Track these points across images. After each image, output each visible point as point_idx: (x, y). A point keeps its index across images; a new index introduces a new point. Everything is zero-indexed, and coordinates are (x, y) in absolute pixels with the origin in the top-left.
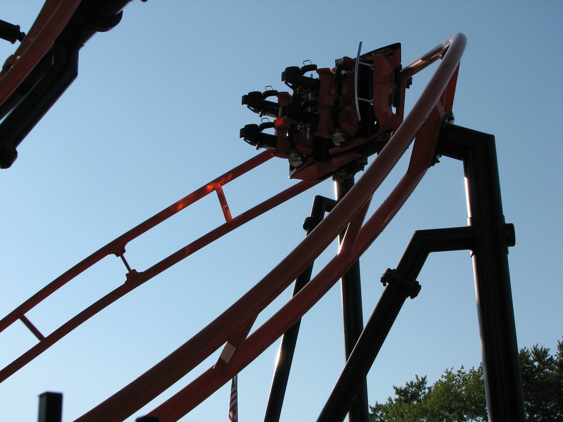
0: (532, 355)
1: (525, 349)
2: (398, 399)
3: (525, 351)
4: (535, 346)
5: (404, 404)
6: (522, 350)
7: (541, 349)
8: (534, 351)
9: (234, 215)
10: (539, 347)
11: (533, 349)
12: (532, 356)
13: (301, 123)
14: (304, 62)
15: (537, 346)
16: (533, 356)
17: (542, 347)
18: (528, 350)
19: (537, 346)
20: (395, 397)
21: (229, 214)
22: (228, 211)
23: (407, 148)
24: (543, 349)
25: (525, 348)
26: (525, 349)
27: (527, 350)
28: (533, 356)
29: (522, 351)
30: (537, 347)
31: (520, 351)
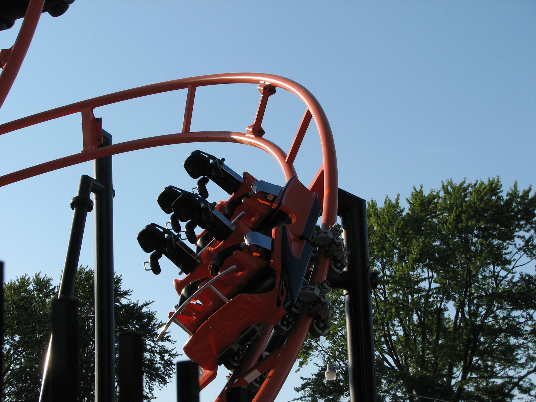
0: (33, 283)
1: (25, 276)
2: (509, 343)
3: (27, 278)
4: (37, 275)
5: (526, 353)
6: (23, 277)
7: (44, 279)
8: (35, 279)
9: (193, 129)
10: (42, 276)
11: (35, 277)
12: (32, 285)
13: (394, 354)
14: (166, 223)
15: (39, 274)
16: (34, 285)
17: (45, 276)
18: (29, 277)
19: (39, 274)
20: (380, 205)
21: (454, 329)
22: (188, 107)
23: (389, 365)
24: (45, 279)
25: (26, 275)
26: (25, 276)
27: (28, 278)
28: (34, 285)
29: (23, 279)
30: (40, 275)
31: (21, 278)
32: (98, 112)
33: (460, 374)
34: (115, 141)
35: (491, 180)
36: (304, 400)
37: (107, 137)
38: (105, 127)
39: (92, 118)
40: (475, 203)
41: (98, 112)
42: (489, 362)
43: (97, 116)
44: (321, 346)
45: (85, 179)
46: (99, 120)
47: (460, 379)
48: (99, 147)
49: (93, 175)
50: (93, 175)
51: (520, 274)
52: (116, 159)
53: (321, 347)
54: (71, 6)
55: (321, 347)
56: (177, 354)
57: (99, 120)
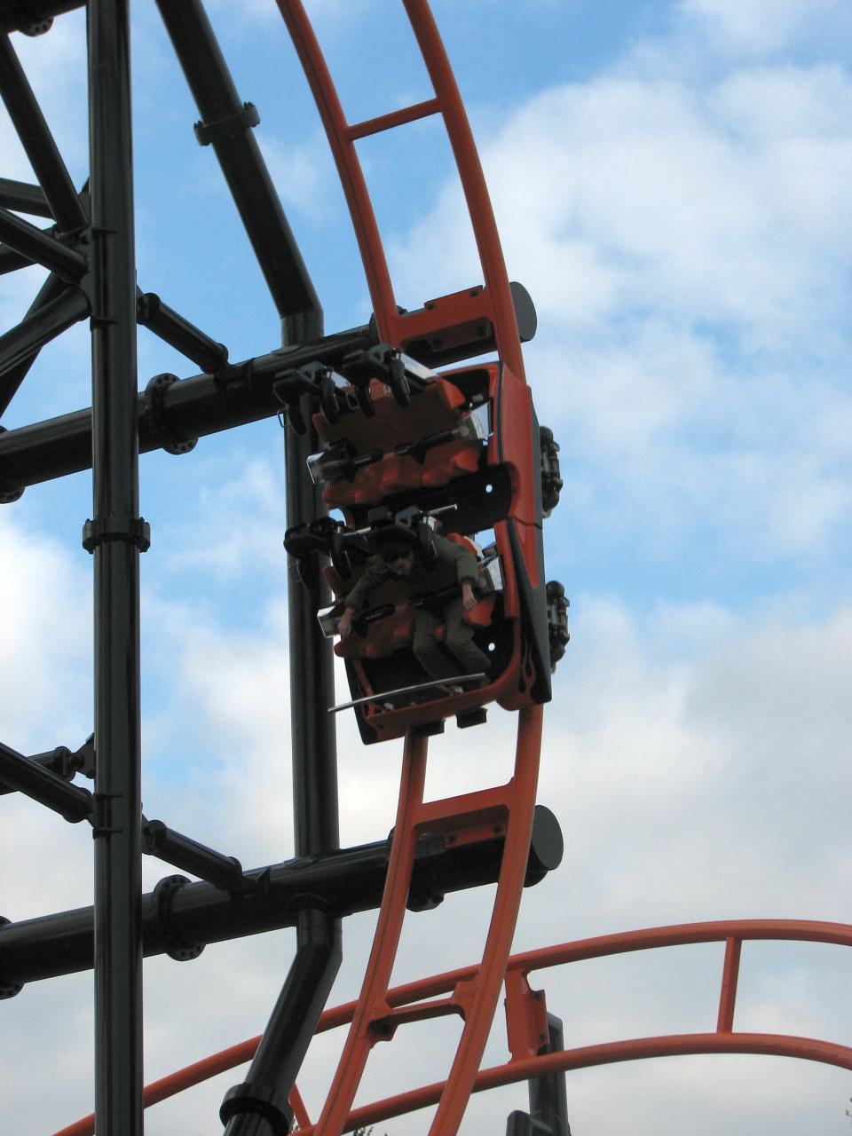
32: (537, 979)
34: (573, 1040)
37: (555, 1031)
38: (552, 1007)
41: (537, 979)
43: (535, 987)
46: (540, 996)
48: (541, 1052)
49: (526, 1107)
50: (526, 1107)
52: (577, 1084)
54: (550, 873)
57: (540, 996)
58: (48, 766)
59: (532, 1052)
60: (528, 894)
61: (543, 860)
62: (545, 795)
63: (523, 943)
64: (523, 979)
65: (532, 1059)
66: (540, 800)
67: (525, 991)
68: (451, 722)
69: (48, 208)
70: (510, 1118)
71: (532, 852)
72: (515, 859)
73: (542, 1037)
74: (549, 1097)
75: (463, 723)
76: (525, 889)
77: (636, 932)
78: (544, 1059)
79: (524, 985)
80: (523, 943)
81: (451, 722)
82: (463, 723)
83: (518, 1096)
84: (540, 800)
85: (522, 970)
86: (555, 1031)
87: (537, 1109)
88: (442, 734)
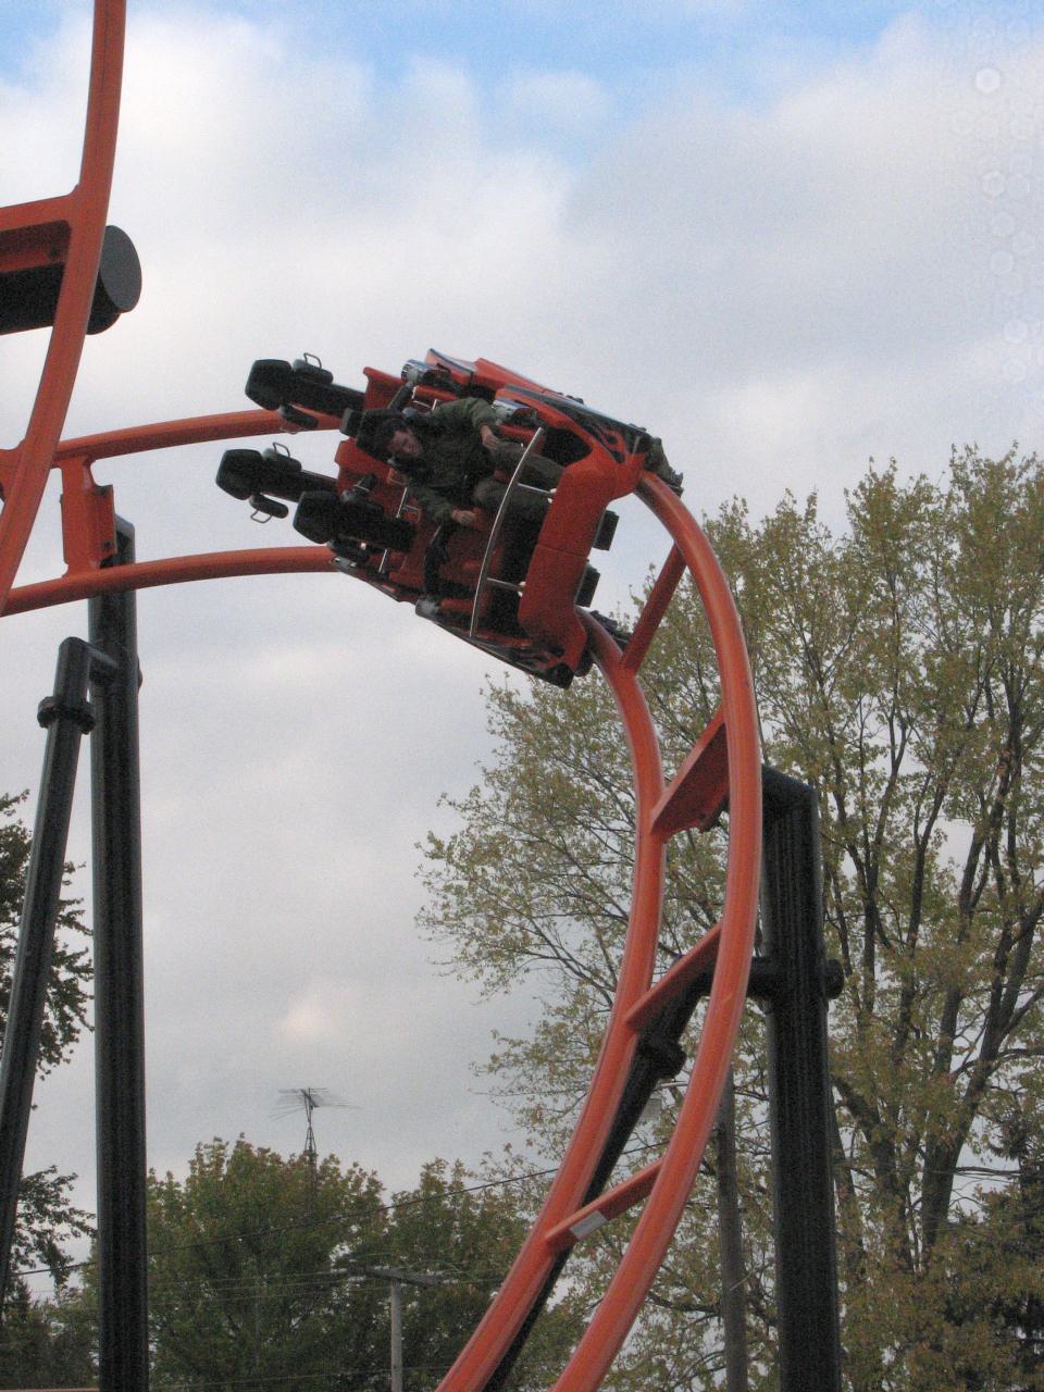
32: (104, 471)
33: (977, 1040)
34: (146, 552)
35: (610, 948)
36: (107, 1328)
37: (124, 541)
38: (123, 508)
39: (87, 485)
40: (845, 741)
41: (104, 471)
42: (735, 1077)
44: (554, 942)
45: (71, 649)
46: (106, 493)
47: (976, 1055)
48: (106, 563)
49: (83, 633)
50: (83, 633)
51: (351, 1167)
52: (149, 602)
53: (553, 947)
54: (123, 316)
55: (553, 947)
56: (11, 797)
57: (106, 493)
58: (467, 628)
59: (94, 564)
60: (93, 344)
61: (112, 293)
62: (119, 214)
63: (78, 424)
64: (84, 469)
65: (94, 573)
66: (112, 220)
67: (87, 485)
68: (596, 558)
69: (597, 1196)
70: (62, 646)
71: (100, 288)
72: (76, 293)
73: (108, 546)
74: (115, 621)
75: (605, 543)
76: (88, 338)
77: (183, 421)
78: (110, 572)
79: (86, 476)
80: (78, 424)
81: (596, 558)
82: (605, 543)
83: (74, 619)
84: (112, 220)
85: (84, 458)
86: (125, 540)
87: (98, 636)
88: (605, 551)
